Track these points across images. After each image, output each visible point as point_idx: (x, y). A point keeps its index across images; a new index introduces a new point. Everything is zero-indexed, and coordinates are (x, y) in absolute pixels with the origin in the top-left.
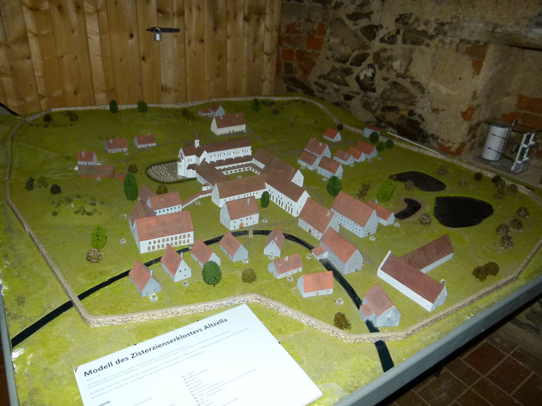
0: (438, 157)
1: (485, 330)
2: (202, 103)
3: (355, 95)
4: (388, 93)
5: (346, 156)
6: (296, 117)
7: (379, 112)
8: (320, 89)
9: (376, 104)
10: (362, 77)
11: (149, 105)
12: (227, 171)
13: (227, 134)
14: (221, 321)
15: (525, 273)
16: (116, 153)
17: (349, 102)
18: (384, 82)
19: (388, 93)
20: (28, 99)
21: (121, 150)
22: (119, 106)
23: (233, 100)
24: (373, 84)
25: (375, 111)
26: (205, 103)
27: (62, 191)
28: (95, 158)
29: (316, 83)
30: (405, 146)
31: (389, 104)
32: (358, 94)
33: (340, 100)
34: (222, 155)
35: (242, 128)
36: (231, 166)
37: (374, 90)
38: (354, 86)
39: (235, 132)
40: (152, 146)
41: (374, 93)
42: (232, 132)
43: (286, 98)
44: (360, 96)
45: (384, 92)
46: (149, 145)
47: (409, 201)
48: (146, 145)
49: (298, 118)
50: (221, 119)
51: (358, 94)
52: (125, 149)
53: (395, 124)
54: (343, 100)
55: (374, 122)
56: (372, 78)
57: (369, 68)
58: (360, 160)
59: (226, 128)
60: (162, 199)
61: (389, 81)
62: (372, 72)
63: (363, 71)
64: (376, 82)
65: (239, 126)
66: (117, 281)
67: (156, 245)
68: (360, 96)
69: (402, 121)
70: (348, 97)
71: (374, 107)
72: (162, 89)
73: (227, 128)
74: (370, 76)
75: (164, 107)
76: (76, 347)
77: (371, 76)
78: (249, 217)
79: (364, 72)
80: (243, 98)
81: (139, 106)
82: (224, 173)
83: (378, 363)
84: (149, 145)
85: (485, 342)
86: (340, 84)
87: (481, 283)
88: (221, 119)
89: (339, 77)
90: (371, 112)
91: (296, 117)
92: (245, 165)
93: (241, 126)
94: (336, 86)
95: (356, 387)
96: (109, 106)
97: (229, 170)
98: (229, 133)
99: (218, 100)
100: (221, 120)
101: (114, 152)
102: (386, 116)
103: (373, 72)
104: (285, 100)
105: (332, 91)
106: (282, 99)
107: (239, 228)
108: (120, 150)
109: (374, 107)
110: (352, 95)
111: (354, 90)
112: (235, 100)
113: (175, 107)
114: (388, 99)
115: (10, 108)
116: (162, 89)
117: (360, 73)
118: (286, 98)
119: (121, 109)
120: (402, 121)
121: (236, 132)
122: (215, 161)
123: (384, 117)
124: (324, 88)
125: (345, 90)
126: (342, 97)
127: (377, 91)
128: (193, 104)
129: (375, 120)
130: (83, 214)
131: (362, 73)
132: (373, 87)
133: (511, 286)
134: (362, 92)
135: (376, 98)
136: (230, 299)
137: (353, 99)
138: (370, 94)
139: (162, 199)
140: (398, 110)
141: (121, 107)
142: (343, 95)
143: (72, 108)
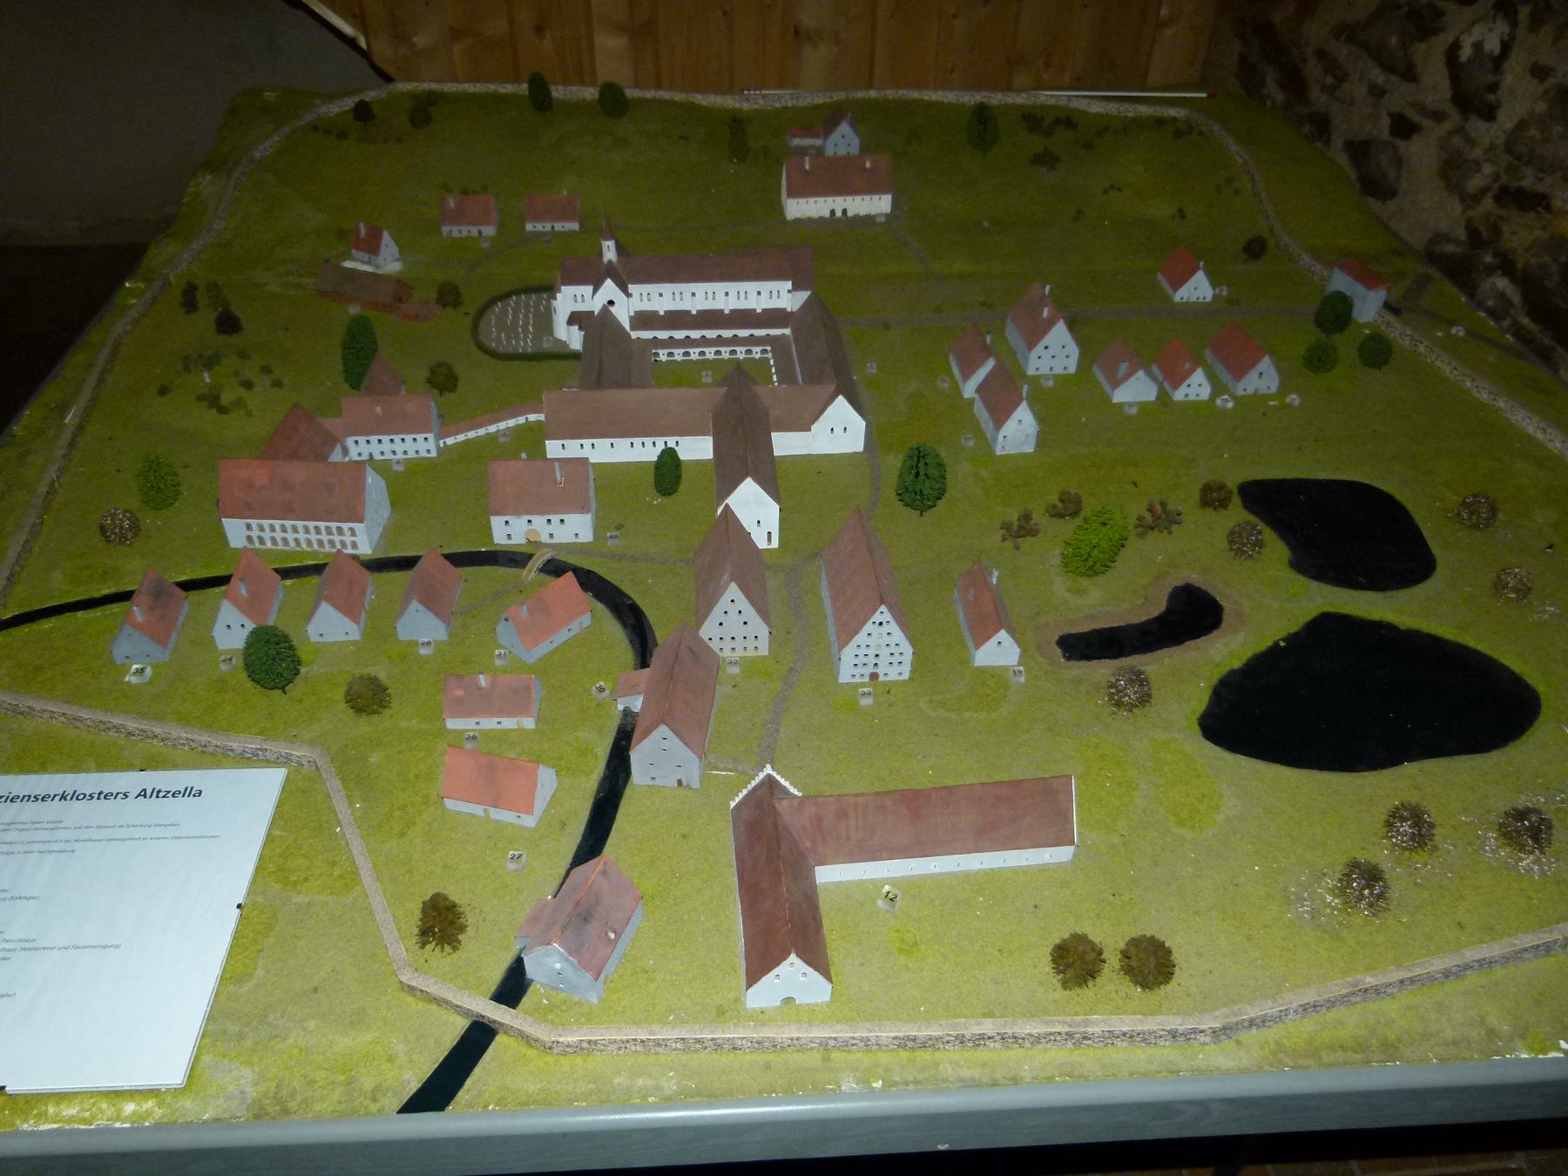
0: (1550, 445)
1: (951, 1149)
2: (827, 100)
3: (1426, 122)
4: (1533, 132)
5: (1123, 368)
6: (1112, 187)
7: (1488, 204)
8: (1329, 80)
9: (1488, 169)
10: (1466, 53)
11: (630, 93)
12: (672, 351)
13: (822, 220)
14: (189, 792)
15: (1301, 1030)
16: (461, 239)
17: (1401, 144)
18: (1535, 82)
19: (1533, 132)
20: (421, 40)
21: (477, 232)
22: (552, 88)
23: (934, 98)
24: (1494, 87)
25: (1476, 198)
26: (835, 99)
27: (244, 324)
28: (388, 246)
29: (1322, 54)
30: (1451, 372)
31: (1528, 181)
32: (1438, 116)
33: (1375, 132)
34: (687, 296)
35: (879, 204)
36: (711, 334)
37: (1489, 114)
38: (1435, 86)
39: (850, 214)
40: (566, 229)
41: (1487, 125)
42: (839, 214)
43: (1133, 106)
44: (1447, 126)
45: (1521, 126)
46: (558, 227)
47: (879, 633)
48: (548, 227)
49: (1120, 190)
50: (807, 167)
51: (1438, 116)
52: (489, 231)
53: (1520, 266)
54: (1385, 134)
55: (1458, 242)
56: (1498, 62)
57: (1495, 16)
58: (1187, 395)
59: (817, 199)
60: (378, 409)
61: (1552, 81)
62: (1503, 33)
63: (1475, 26)
64: (1508, 80)
65: (867, 198)
66: (108, 607)
67: (267, 535)
68: (1447, 126)
69: (1547, 259)
70: (1403, 128)
71: (1475, 183)
72: (797, 33)
73: (821, 200)
74: (1492, 51)
75: (704, 103)
76: (1499, 588)
77: (1497, 51)
78: (555, 518)
79: (1477, 32)
80: (972, 96)
81: (602, 94)
82: (663, 355)
83: (413, 1080)
84: (558, 227)
85: (1513, 1166)
86: (1389, 69)
87: (1060, 994)
88: (807, 167)
89: (1394, 41)
90: (1463, 200)
91: (1112, 187)
92: (744, 338)
93: (876, 197)
94: (1377, 75)
95: (286, 1111)
96: (525, 86)
97: (694, 347)
98: (827, 214)
99: (882, 94)
100: (806, 171)
101: (456, 234)
102: (1505, 228)
103: (1506, 38)
104: (1130, 115)
105: (1363, 90)
106: (1118, 110)
107: (523, 541)
108: (474, 231)
109: (1475, 183)
110: (1416, 118)
111: (1430, 100)
112: (994, 96)
113: (738, 106)
114: (1526, 159)
115: (378, 62)
116: (797, 33)
117: (1463, 32)
118: (1135, 109)
119: (581, 97)
120: (1547, 259)
121: (856, 217)
122: (662, 313)
123: (1496, 231)
124: (1342, 77)
125: (1400, 96)
126: (1385, 122)
127: (1498, 117)
128: (794, 102)
129: (1462, 234)
130: (210, 406)
131: (1470, 34)
132: (1491, 97)
133: (1167, 1053)
134: (1454, 115)
135: (1492, 148)
136: (250, 743)
137: (1415, 137)
138: (1477, 126)
139: (378, 409)
140: (1549, 209)
141: (558, 92)
142: (1390, 115)
143: (449, 85)
